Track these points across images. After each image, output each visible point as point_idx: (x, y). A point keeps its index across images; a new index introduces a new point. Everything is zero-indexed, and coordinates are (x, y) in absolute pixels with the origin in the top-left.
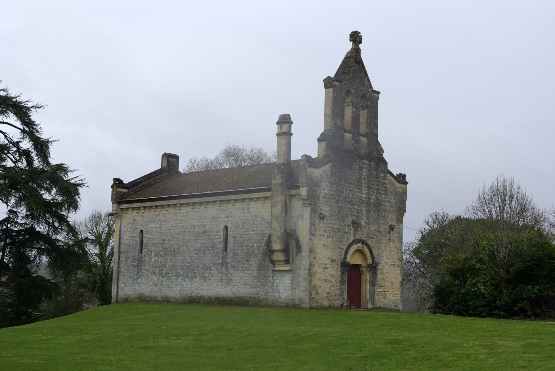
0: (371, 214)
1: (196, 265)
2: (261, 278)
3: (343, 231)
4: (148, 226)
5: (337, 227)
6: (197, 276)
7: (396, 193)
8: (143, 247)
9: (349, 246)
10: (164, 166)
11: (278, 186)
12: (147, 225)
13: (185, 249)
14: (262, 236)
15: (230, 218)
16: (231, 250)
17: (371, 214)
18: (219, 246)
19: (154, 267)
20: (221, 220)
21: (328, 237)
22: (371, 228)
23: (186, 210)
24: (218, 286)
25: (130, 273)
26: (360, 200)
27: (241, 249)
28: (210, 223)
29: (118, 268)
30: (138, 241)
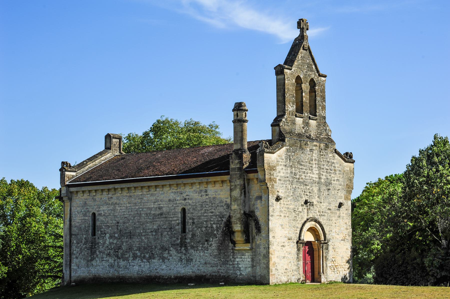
0: (322, 193)
1: (153, 247)
2: (221, 257)
3: (298, 211)
4: (101, 209)
5: (292, 207)
6: (155, 257)
7: (344, 171)
8: (96, 230)
9: (303, 225)
10: (108, 147)
11: (237, 171)
12: (100, 208)
13: (142, 231)
14: (220, 218)
15: (187, 201)
16: (189, 231)
17: (322, 193)
18: (177, 227)
19: (109, 249)
20: (177, 202)
21: (285, 216)
22: (322, 206)
23: (141, 193)
24: (178, 266)
25: (83, 255)
26: (312, 181)
27: (200, 230)
28: (166, 206)
29: (70, 250)
30: (90, 223)
